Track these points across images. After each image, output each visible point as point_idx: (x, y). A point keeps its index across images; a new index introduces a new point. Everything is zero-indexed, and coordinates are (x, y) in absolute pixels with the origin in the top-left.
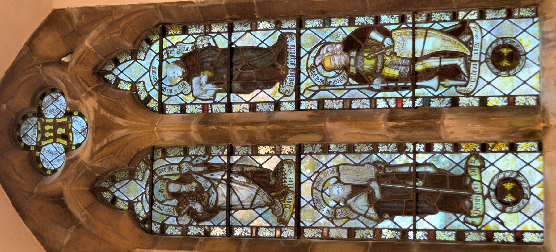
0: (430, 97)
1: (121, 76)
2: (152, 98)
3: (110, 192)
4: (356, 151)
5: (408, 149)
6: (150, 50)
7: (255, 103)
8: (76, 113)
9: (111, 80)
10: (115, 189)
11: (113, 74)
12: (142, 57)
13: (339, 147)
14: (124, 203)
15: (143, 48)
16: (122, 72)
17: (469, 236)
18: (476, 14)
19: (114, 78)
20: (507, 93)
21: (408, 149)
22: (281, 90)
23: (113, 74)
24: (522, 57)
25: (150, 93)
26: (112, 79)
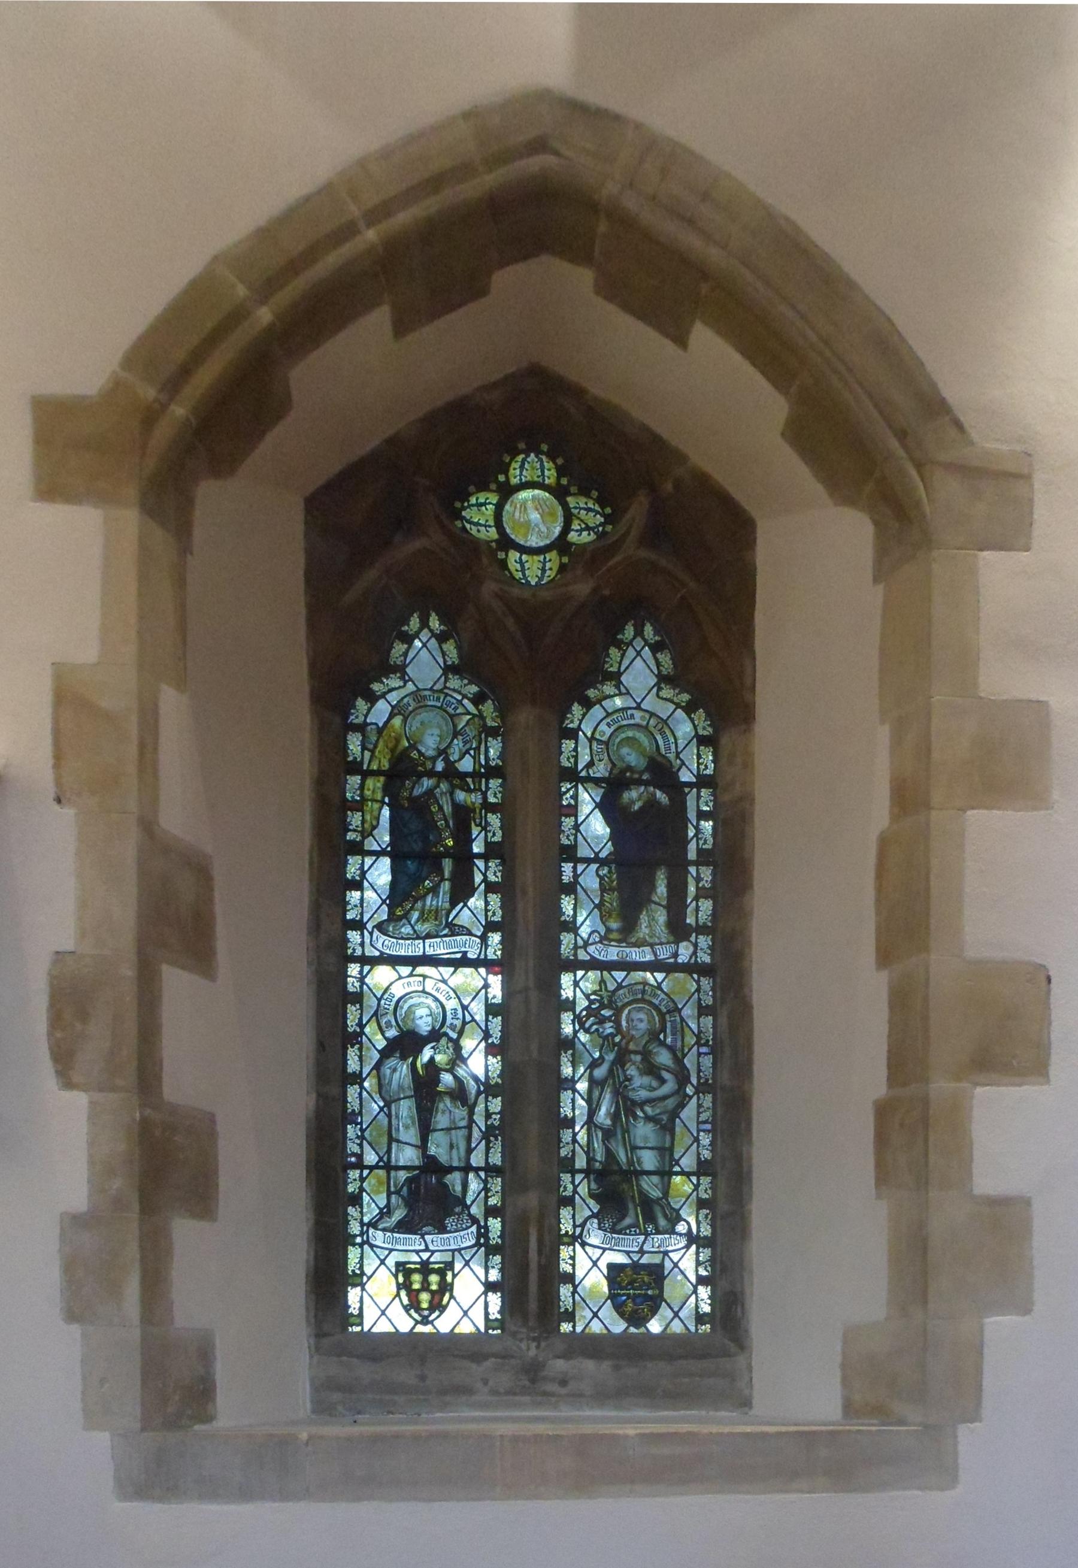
0: (576, 817)
1: (631, 653)
2: (588, 711)
3: (421, 630)
4: (490, 1057)
5: (493, 1018)
6: (674, 707)
7: (575, 892)
8: (565, 560)
9: (624, 634)
10: (424, 640)
11: (634, 638)
12: (664, 694)
13: (496, 869)
14: (400, 656)
15: (679, 693)
16: (639, 653)
17: (354, 1008)
18: (707, 1274)
19: (627, 639)
20: (580, 880)
21: (493, 1018)
22: (596, 934)
23: (634, 638)
24: (633, 1056)
25: (598, 706)
26: (626, 636)
